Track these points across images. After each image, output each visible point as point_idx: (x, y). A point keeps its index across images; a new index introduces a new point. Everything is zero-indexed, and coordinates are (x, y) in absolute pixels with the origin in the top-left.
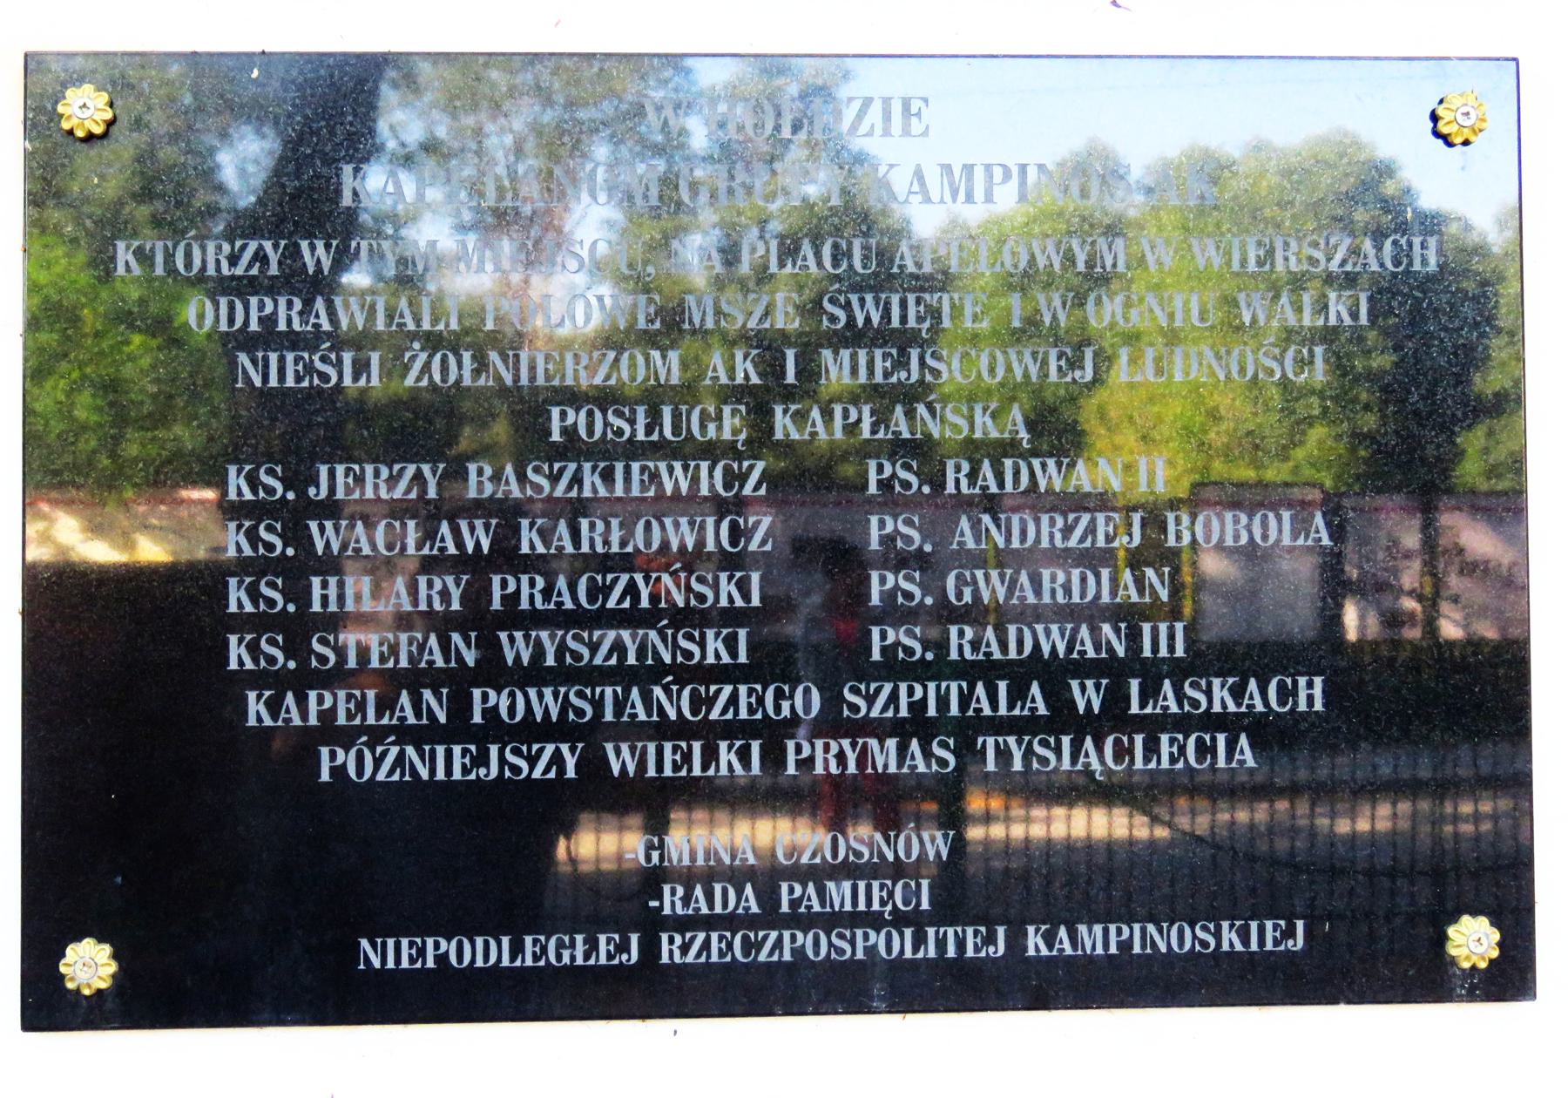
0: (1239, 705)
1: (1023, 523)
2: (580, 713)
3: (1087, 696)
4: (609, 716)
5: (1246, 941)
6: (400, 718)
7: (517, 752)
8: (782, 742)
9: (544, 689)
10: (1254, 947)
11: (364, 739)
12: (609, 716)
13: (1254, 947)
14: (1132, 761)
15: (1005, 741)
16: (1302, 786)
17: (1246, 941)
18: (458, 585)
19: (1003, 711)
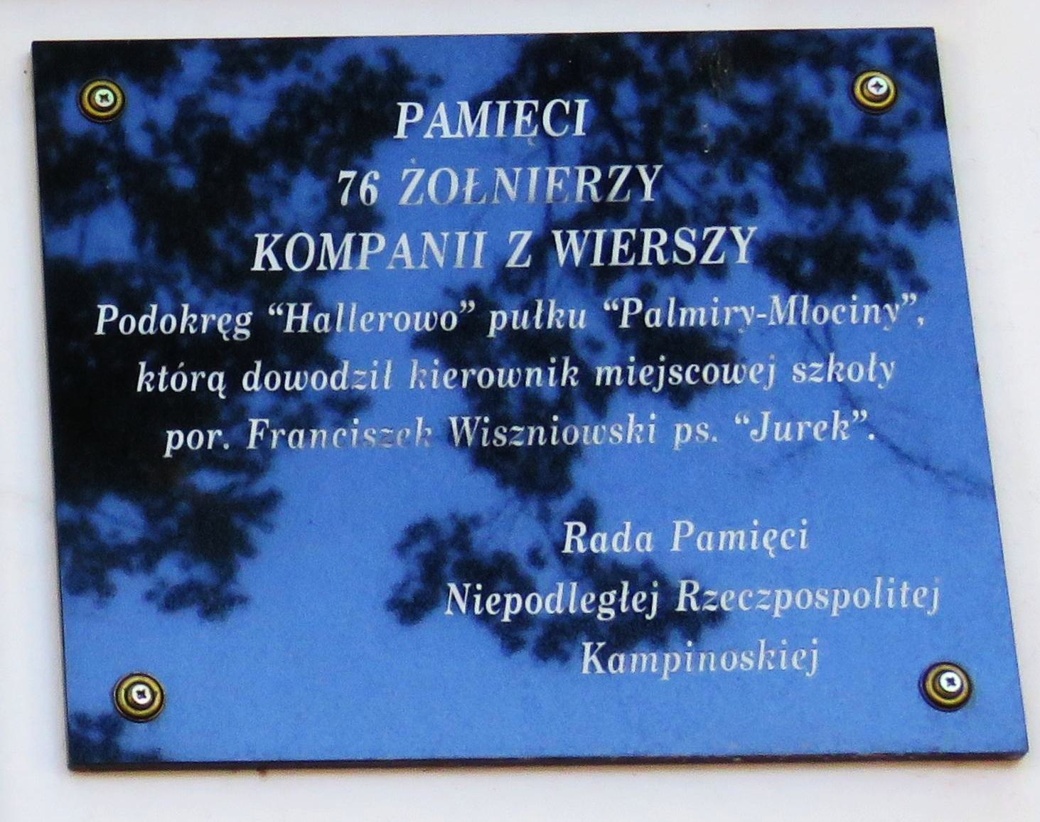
14: (573, 130)
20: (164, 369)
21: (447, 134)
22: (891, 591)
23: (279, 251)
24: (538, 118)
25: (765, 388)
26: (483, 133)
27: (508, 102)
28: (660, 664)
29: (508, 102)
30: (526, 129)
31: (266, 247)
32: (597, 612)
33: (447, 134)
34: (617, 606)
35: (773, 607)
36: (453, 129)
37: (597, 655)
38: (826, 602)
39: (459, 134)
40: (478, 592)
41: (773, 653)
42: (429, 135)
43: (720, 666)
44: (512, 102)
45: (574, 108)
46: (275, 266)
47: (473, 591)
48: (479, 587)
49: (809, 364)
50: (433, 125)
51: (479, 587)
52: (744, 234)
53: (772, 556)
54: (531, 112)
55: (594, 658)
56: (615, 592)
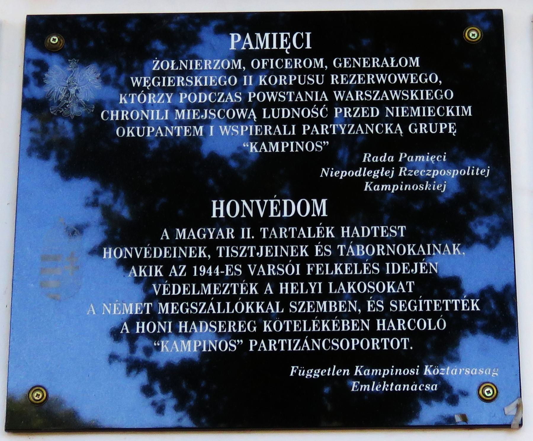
0: (396, 290)
1: (289, 204)
2: (282, 99)
3: (246, 233)
4: (290, 100)
5: (148, 273)
6: (228, 100)
7: (234, 249)
8: (334, 264)
9: (339, 91)
10: (422, 98)
11: (143, 91)
12: (290, 100)
13: (422, 98)
14: (305, 45)
15: (234, 100)
16: (133, 345)
17: (148, 273)
18: (212, 231)
19: (309, 236)
20: (392, 383)
21: (251, 48)
22: (473, 171)
23: (267, 80)
24: (290, 40)
25: (390, 177)
26: (267, 47)
27: (270, 33)
28: (392, 188)
29: (277, 33)
30: (286, 46)
31: (262, 79)
32: (373, 176)
33: (251, 48)
34: (379, 174)
35: (432, 175)
36: (254, 46)
37: (370, 186)
38: (450, 173)
39: (257, 48)
40: (332, 170)
41: (430, 186)
42: (243, 48)
43: (430, 159)
44: (271, 33)
45: (305, 36)
46: (265, 84)
47: (330, 170)
48: (333, 169)
49: (413, 175)
50: (245, 43)
51: (333, 169)
53: (433, 163)
54: (287, 38)
55: (369, 186)
56: (379, 170)
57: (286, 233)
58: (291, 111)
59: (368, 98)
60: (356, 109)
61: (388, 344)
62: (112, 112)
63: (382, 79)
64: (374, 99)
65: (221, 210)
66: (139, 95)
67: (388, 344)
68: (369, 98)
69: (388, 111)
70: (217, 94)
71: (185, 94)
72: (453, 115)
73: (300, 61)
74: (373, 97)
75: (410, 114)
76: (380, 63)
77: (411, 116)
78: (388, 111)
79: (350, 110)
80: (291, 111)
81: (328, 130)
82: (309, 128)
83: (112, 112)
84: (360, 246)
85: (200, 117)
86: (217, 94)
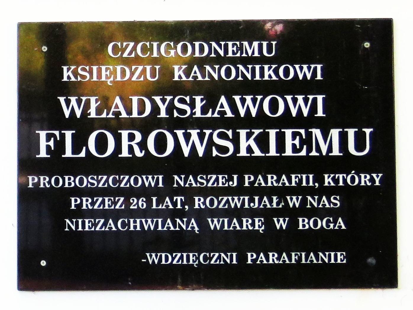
24: (198, 258)
52: (378, 176)
57: (369, 180)
58: (210, 46)
59: (202, 184)
60: (97, 200)
61: (345, 180)
62: (132, 221)
63: (150, 182)
64: (210, 185)
65: (67, 180)
66: (350, 176)
67: (345, 180)
68: (203, 184)
69: (179, 223)
70: (119, 178)
71: (71, 177)
72: (257, 153)
73: (47, 179)
74: (98, 184)
75: (309, 150)
76: (278, 181)
77: (314, 153)
78: (179, 224)
79: (90, 200)
80: (210, 46)
81: (369, 180)
82: (252, 178)
83: (132, 221)
84: (32, 178)
85: (229, 184)
86: (119, 178)
